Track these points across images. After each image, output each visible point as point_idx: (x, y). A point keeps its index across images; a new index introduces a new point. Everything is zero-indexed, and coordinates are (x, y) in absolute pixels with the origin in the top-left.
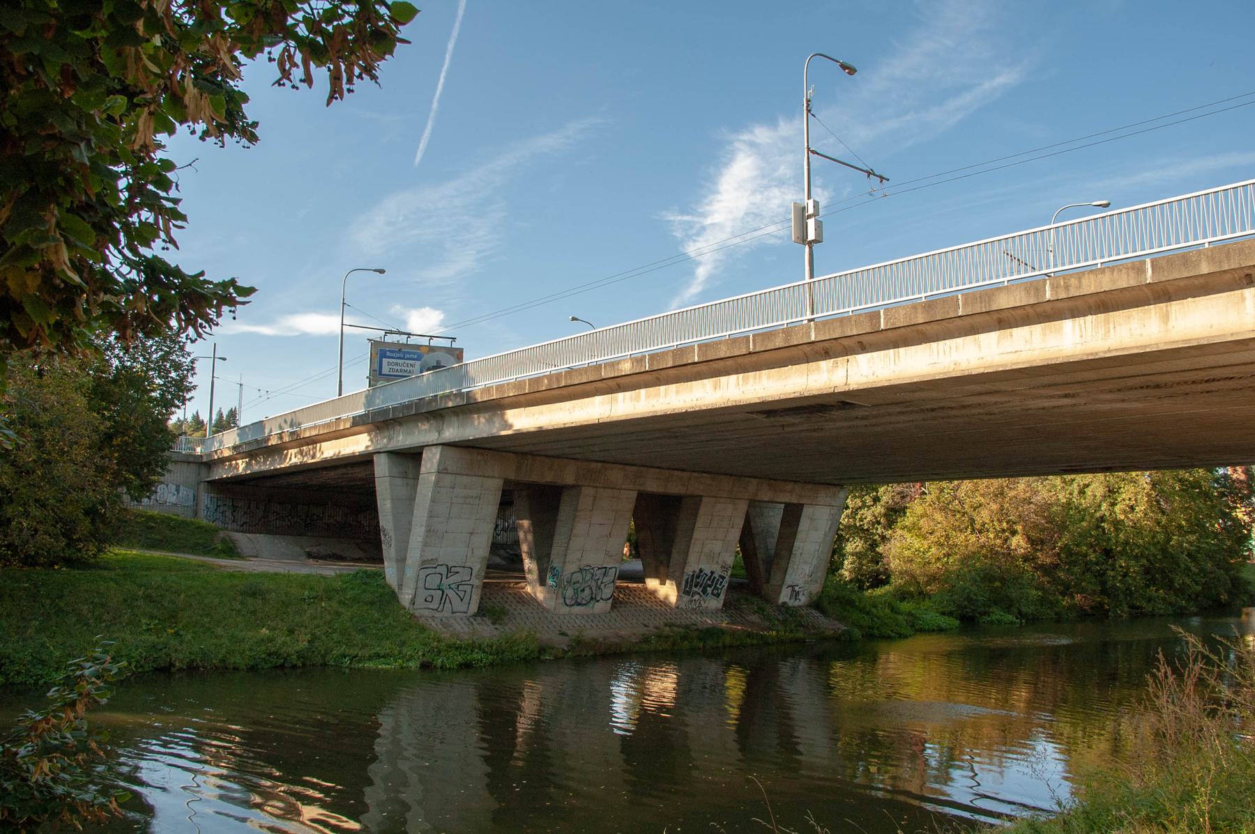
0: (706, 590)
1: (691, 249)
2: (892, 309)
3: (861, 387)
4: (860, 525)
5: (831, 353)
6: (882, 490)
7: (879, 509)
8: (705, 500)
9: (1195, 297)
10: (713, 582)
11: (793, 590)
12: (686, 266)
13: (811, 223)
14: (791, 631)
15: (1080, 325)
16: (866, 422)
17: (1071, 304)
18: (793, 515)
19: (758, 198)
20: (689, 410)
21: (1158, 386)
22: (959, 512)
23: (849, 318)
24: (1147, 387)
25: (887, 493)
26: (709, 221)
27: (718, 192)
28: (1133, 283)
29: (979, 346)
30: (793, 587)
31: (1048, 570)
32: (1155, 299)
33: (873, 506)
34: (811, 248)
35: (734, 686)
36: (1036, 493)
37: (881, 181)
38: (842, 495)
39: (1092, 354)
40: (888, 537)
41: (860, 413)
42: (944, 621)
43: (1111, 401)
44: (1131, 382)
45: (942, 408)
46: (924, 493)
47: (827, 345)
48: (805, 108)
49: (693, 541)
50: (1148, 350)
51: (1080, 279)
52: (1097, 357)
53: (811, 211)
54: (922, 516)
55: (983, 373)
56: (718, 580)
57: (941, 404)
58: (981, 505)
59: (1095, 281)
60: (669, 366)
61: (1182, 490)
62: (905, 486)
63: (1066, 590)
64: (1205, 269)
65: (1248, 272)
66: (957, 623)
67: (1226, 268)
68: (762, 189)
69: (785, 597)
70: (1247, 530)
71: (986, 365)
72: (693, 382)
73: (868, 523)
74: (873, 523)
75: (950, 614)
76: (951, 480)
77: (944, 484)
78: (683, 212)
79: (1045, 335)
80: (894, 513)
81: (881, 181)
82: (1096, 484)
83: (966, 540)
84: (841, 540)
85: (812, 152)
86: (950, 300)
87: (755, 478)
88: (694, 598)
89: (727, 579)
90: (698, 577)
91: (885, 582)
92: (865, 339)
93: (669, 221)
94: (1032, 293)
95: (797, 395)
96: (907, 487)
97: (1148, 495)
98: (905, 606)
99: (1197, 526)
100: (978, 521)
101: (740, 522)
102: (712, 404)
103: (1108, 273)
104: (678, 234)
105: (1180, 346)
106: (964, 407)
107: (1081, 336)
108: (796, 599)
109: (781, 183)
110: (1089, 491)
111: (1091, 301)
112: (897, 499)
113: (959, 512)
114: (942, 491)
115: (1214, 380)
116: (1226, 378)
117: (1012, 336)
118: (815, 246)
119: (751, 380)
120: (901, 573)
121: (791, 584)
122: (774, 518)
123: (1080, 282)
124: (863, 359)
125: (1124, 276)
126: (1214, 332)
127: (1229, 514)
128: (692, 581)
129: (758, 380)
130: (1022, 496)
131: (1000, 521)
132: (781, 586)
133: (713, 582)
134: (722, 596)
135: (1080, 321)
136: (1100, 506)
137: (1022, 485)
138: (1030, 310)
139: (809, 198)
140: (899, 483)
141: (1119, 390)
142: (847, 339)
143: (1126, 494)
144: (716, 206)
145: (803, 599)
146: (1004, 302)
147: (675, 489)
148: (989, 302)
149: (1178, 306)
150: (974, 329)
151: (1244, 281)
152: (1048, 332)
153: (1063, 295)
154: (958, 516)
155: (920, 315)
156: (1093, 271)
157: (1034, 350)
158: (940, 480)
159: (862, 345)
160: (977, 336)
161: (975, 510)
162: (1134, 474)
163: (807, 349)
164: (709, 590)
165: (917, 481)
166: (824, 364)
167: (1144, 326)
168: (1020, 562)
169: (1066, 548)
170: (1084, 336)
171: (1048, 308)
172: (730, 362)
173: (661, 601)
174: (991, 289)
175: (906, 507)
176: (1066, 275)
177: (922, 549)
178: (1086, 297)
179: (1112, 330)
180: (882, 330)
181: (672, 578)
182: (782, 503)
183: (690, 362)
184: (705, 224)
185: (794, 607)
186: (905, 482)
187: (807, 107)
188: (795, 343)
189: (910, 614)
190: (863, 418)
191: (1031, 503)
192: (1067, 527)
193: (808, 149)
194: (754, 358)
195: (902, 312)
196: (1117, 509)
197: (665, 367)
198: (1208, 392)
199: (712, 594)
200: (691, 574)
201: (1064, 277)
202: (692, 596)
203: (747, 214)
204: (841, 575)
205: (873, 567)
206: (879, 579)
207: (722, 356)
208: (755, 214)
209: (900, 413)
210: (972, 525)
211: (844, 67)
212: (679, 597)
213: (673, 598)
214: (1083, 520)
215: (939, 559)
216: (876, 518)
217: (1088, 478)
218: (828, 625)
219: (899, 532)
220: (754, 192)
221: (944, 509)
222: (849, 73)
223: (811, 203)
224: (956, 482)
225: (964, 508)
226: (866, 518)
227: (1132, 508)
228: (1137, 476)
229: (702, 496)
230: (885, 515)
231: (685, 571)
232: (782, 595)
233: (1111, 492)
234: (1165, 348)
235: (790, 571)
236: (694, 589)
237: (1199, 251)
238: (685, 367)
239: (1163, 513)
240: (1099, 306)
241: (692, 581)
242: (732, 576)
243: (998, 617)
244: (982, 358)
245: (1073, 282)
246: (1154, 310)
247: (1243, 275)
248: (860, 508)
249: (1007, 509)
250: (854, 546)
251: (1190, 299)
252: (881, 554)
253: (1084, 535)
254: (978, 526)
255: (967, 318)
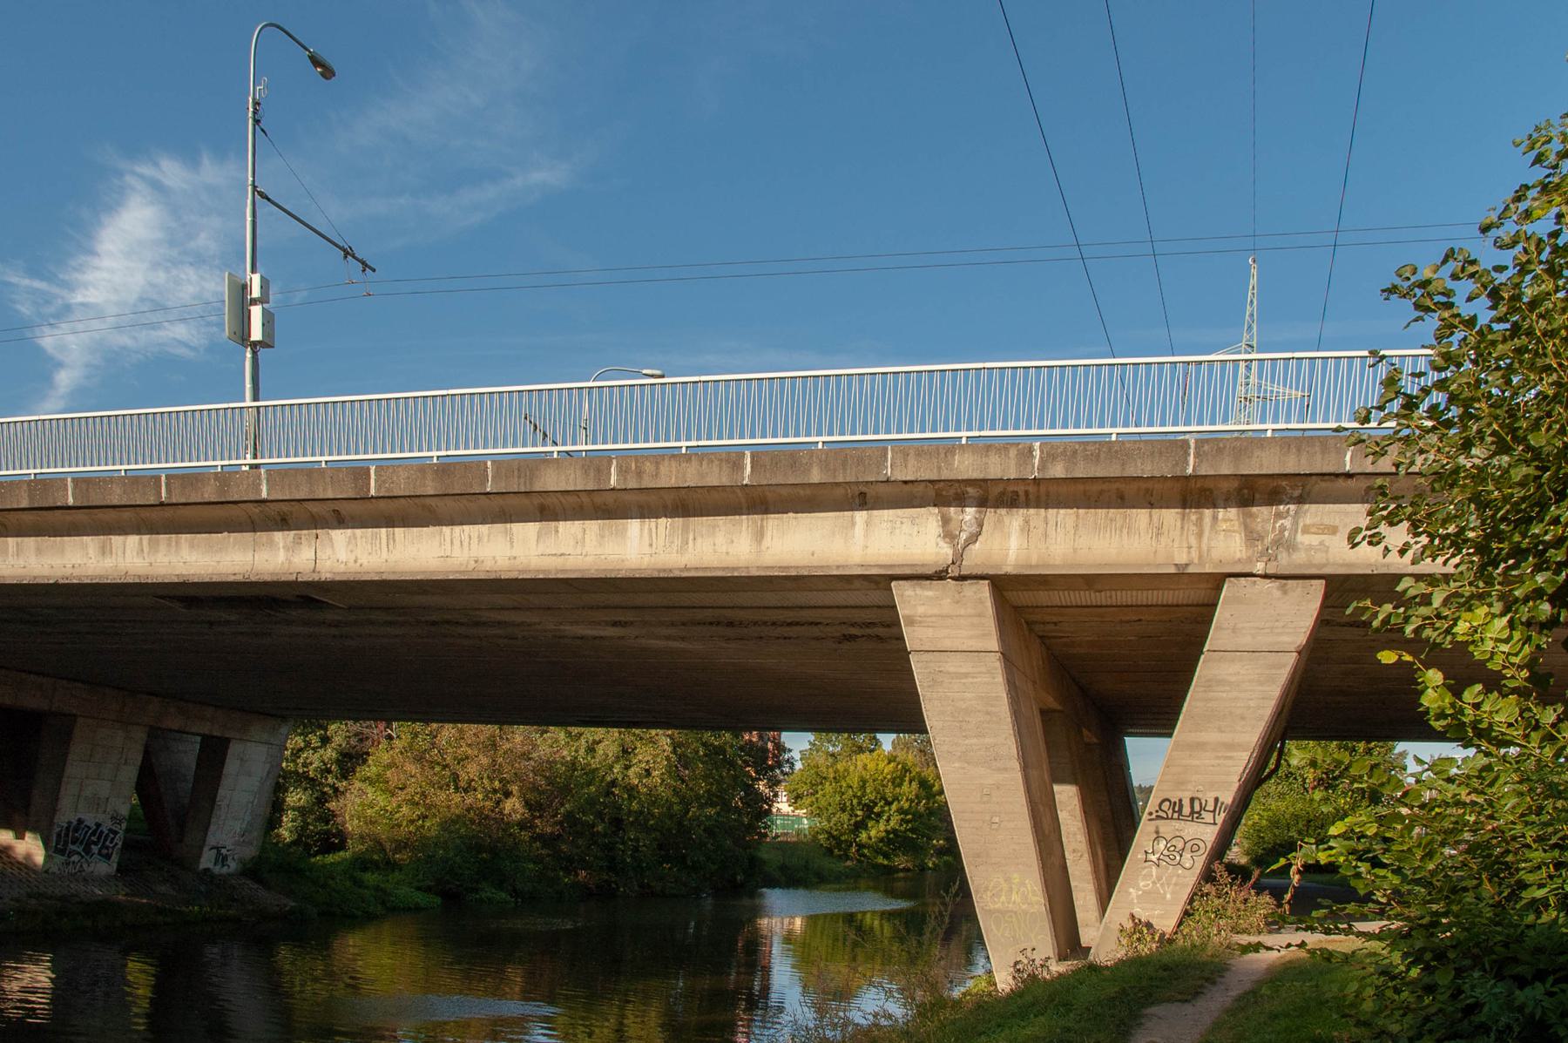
0: (90, 849)
1: (47, 341)
2: (388, 467)
3: (338, 578)
4: (304, 772)
5: (290, 522)
6: (333, 727)
7: (330, 753)
8: (80, 720)
9: (797, 512)
10: (99, 838)
11: (219, 853)
12: (42, 368)
13: (256, 312)
14: (220, 907)
15: (650, 530)
16: (333, 631)
17: (642, 498)
18: (214, 754)
19: (161, 277)
20: (61, 581)
21: (731, 624)
22: (438, 764)
23: (321, 472)
24: (718, 623)
25: (340, 732)
26: (78, 298)
27: (93, 253)
28: (725, 481)
29: (512, 543)
30: (217, 848)
31: (549, 841)
32: (748, 508)
33: (321, 747)
34: (254, 353)
35: (139, 975)
36: (535, 746)
37: (364, 271)
38: (284, 730)
39: (664, 570)
40: (341, 789)
41: (330, 616)
42: (421, 898)
43: (668, 638)
44: (700, 615)
45: (448, 622)
46: (390, 737)
47: (285, 508)
48: (250, 114)
49: (65, 779)
50: (736, 574)
51: (657, 463)
52: (671, 575)
53: (256, 293)
54: (389, 766)
55: (517, 579)
56: (107, 835)
57: (448, 617)
58: (467, 758)
59: (678, 471)
60: (22, 506)
61: (705, 755)
62: (364, 725)
63: (570, 865)
64: (816, 476)
65: (864, 489)
66: (438, 900)
67: (841, 479)
68: (169, 264)
69: (207, 861)
70: (768, 805)
71: (520, 568)
72: (66, 539)
73: (315, 770)
74: (321, 770)
75: (428, 890)
76: (427, 721)
77: (418, 726)
78: (34, 273)
79: (603, 537)
80: (350, 761)
81: (364, 271)
82: (608, 741)
83: (451, 801)
84: (279, 789)
85: (262, 195)
86: (474, 467)
87: (157, 696)
88: (73, 859)
89: (121, 834)
90: (76, 830)
91: (342, 846)
92: (345, 508)
93: (8, 284)
94: (592, 474)
95: (239, 578)
96: (367, 727)
97: (668, 758)
98: (370, 878)
99: (718, 798)
100: (463, 776)
101: (138, 758)
102: (101, 577)
103: (695, 462)
104: (25, 309)
105: (776, 574)
106: (477, 624)
107: (651, 545)
108: (223, 866)
109: (199, 260)
110: (600, 749)
111: (669, 498)
112: (353, 741)
113: (438, 764)
114: (416, 735)
115: (797, 624)
116: (811, 623)
117: (557, 531)
118: (262, 352)
119: (163, 548)
120: (362, 837)
121: (215, 844)
122: (187, 755)
123: (657, 468)
124: (339, 536)
125: (716, 469)
126: (815, 561)
127: (752, 786)
128: (67, 835)
129: (173, 549)
130: (520, 749)
131: (491, 779)
132: (201, 848)
133: (99, 838)
134: (115, 858)
135: (651, 523)
136: (611, 767)
137: (518, 736)
138: (585, 499)
139: (253, 271)
140: (356, 720)
141: (684, 624)
142: (317, 503)
143: (643, 754)
144: (90, 276)
145: (233, 866)
146: (551, 481)
147: (32, 701)
148: (531, 479)
149: (776, 522)
150: (505, 514)
151: (857, 501)
152: (607, 533)
153: (632, 484)
154: (437, 769)
155: (429, 483)
156: (674, 455)
157: (586, 555)
158: (414, 721)
159: (337, 514)
160: (508, 525)
161: (459, 763)
162: (653, 732)
163: (255, 510)
164: (95, 849)
165: (381, 720)
166: (279, 537)
167: (732, 542)
168: (516, 830)
169: (569, 816)
170: (654, 546)
171: (609, 499)
172: (127, 515)
173: (19, 863)
174: (535, 461)
175: (368, 754)
176: (640, 456)
177: (388, 808)
178: (662, 492)
179: (691, 542)
180: (372, 497)
181: (34, 830)
182: (198, 735)
183: (59, 504)
184: (73, 301)
185: (221, 875)
186: (365, 719)
187: (255, 113)
188: (236, 498)
189: (377, 888)
190: (337, 625)
191: (530, 759)
192: (571, 790)
193: (254, 187)
194: (168, 513)
195: (403, 474)
196: (631, 772)
197: (15, 506)
198: (785, 638)
199: (100, 853)
200: (66, 825)
201: (637, 459)
202: (69, 857)
203: (142, 300)
204: (278, 836)
205: (321, 827)
206: (333, 841)
207: (115, 502)
208: (153, 307)
209: (390, 623)
210: (455, 781)
211: (316, 61)
212: (48, 857)
213: (39, 857)
214: (589, 784)
215: (412, 822)
216: (325, 764)
217: (600, 732)
218: (271, 899)
219: (358, 784)
220: (155, 266)
221: (419, 759)
222: (322, 74)
223: (256, 279)
224: (435, 725)
225: (445, 759)
226: (311, 764)
227: (648, 772)
228: (657, 735)
229: (75, 715)
230: (338, 761)
231: (55, 821)
232: (202, 860)
233: (626, 752)
234: (758, 574)
235: (212, 828)
236: (71, 847)
237: (811, 453)
238: (50, 513)
239: (683, 781)
240: (677, 506)
241: (67, 835)
242: (127, 830)
243: (488, 894)
244: (515, 558)
245: (649, 467)
246: (745, 522)
247: (857, 493)
248: (301, 750)
249: (500, 765)
250: (296, 797)
251: (791, 515)
252: (333, 811)
253: (592, 802)
254: (462, 784)
255: (497, 497)
